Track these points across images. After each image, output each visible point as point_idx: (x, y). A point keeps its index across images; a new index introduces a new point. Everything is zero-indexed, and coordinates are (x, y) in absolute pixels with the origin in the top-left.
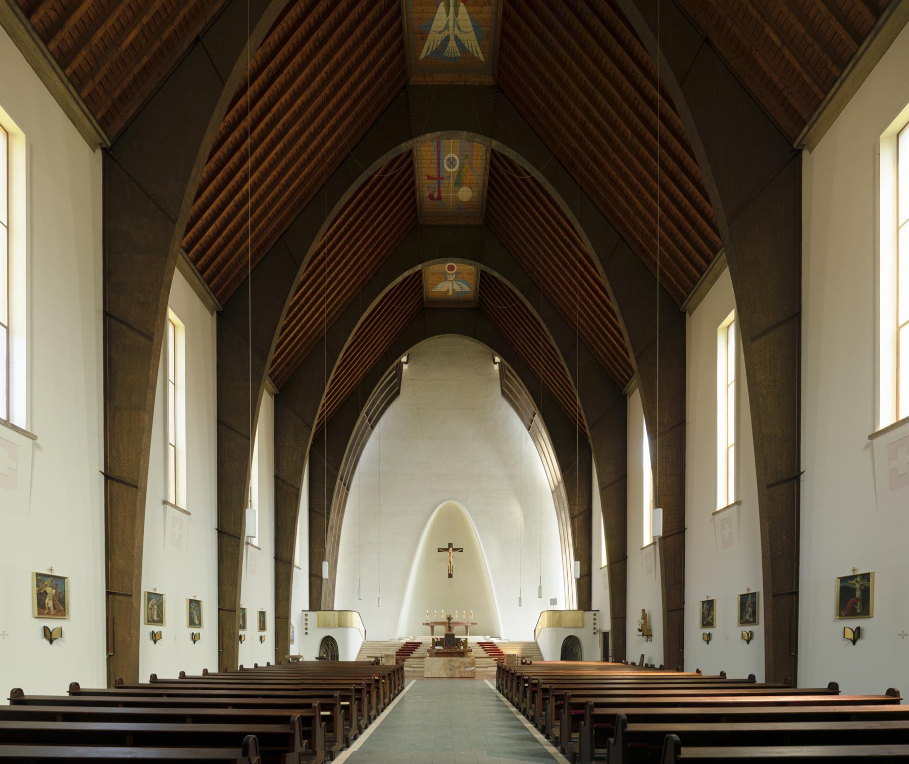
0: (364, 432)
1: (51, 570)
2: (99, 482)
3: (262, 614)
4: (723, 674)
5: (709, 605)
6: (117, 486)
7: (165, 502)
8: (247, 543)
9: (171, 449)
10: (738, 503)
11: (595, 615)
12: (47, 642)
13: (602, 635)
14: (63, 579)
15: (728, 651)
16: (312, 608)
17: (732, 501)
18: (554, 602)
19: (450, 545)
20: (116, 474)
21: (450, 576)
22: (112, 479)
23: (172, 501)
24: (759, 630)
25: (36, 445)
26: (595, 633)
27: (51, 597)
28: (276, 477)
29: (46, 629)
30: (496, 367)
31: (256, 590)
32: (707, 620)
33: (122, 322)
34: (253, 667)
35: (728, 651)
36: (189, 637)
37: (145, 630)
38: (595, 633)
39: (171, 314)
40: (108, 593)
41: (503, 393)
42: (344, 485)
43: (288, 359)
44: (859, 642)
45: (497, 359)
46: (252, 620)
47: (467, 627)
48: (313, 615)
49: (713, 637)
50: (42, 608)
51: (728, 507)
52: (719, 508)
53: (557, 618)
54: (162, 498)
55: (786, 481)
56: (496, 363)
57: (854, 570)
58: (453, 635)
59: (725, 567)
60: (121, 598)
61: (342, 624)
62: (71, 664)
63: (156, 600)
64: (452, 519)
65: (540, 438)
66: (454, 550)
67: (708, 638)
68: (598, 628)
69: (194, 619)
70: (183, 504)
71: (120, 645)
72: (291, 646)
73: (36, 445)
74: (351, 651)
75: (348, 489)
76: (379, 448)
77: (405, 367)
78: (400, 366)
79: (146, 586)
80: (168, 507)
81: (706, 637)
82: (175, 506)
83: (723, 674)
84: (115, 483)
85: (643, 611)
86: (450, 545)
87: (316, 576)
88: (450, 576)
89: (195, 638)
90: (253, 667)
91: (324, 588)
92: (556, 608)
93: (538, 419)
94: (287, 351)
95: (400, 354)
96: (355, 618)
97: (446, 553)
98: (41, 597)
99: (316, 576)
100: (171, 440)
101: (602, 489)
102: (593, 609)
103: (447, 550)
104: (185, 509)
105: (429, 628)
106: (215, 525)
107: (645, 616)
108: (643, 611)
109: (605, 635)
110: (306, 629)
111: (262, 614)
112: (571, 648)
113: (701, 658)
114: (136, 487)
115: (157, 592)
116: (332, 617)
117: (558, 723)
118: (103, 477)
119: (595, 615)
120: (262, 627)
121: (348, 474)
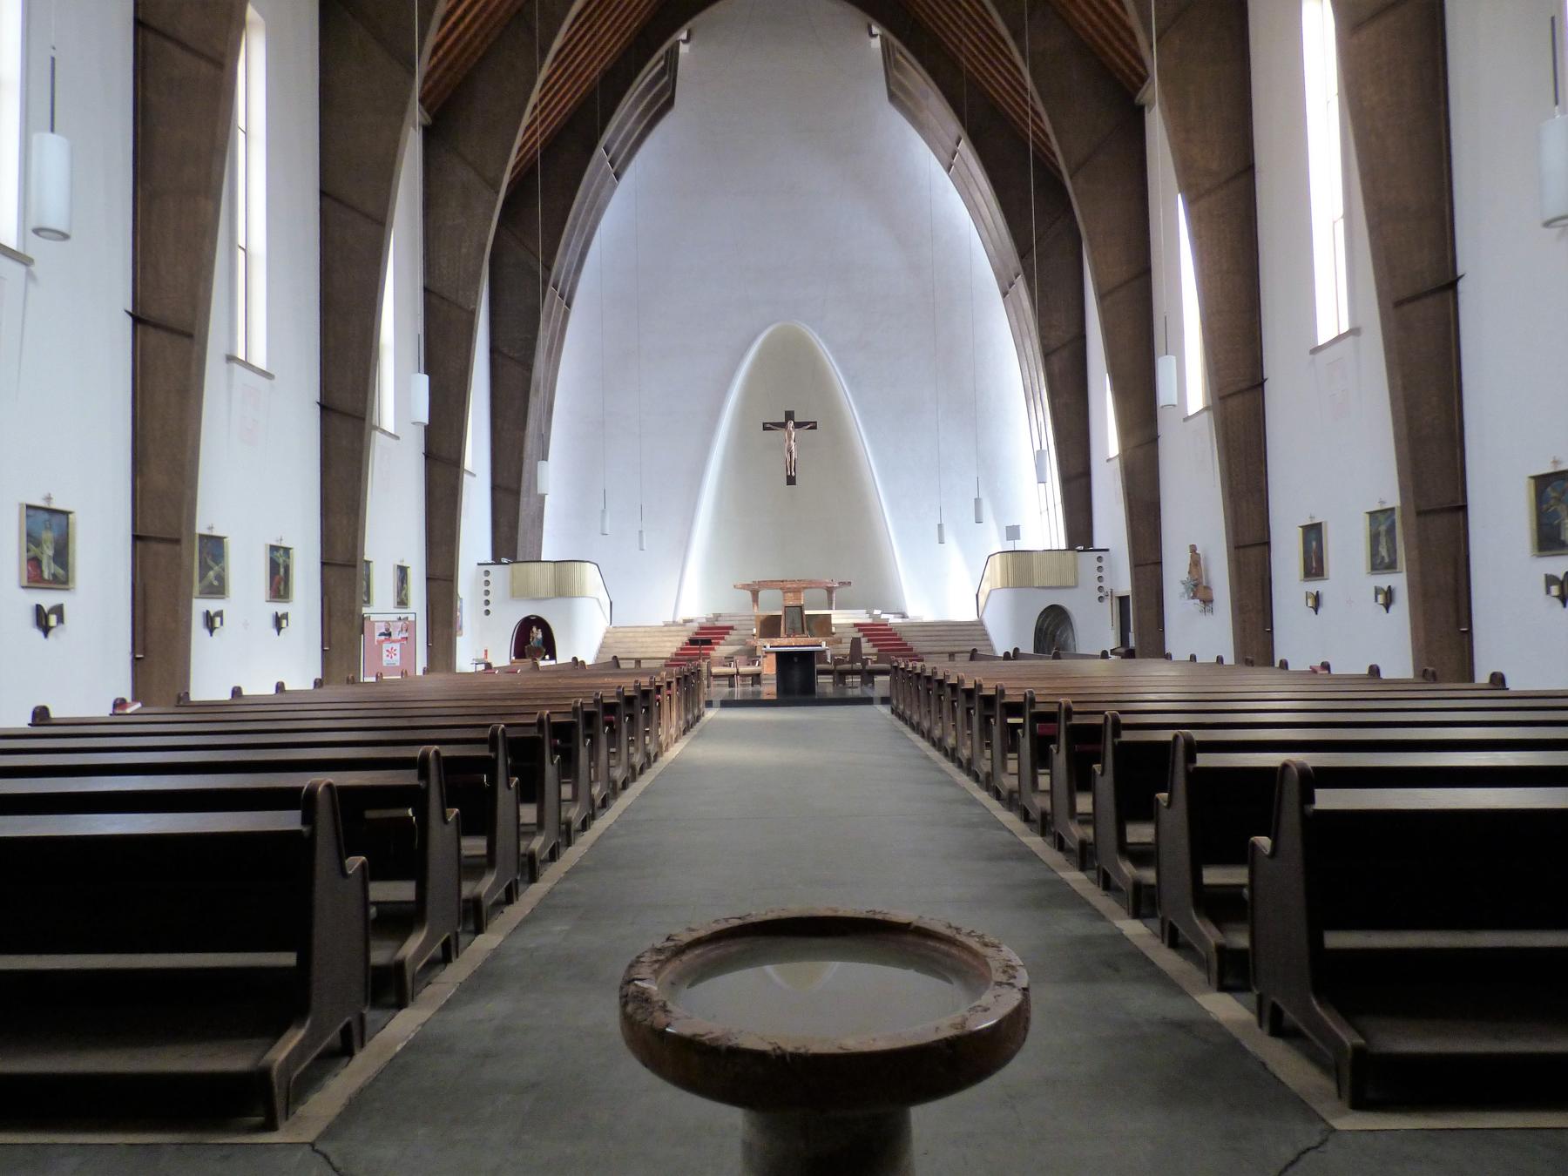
0: (601, 186)
1: (49, 499)
2: (316, 412)
3: (403, 571)
4: (1374, 671)
5: (1313, 533)
6: (154, 337)
7: (231, 358)
8: (376, 428)
9: (241, 254)
10: (1354, 331)
11: (1100, 559)
12: (40, 634)
13: (1116, 603)
14: (66, 513)
15: (1350, 628)
16: (496, 559)
17: (1345, 328)
18: (1013, 532)
19: (789, 415)
20: (154, 312)
21: (791, 481)
22: (334, 411)
23: (241, 355)
24: (1398, 581)
25: (30, 276)
26: (1101, 599)
27: (48, 548)
28: (427, 290)
29: (39, 608)
30: (876, 43)
31: (256, 483)
32: (1314, 567)
33: (352, 208)
34: (227, 696)
35: (1350, 628)
36: (29, 617)
37: (200, 606)
38: (1101, 599)
39: (251, 13)
40: (136, 538)
41: (892, 97)
42: (561, 296)
43: (452, 56)
44: (1392, 608)
45: (875, 30)
46: (246, 571)
47: (830, 590)
48: (500, 573)
49: (1325, 600)
50: (35, 577)
51: (1340, 338)
52: (1323, 337)
53: (1020, 566)
54: (224, 351)
55: (1433, 292)
56: (873, 36)
57: (1382, 502)
58: (801, 608)
59: (1337, 458)
60: (161, 547)
61: (563, 588)
62: (82, 672)
63: (214, 546)
64: (791, 363)
65: (973, 188)
66: (798, 425)
67: (1317, 602)
68: (1107, 589)
69: (279, 584)
70: (259, 359)
71: (158, 640)
72: (459, 639)
73: (30, 276)
74: (582, 639)
75: (569, 305)
76: (629, 216)
77: (684, 49)
78: (673, 54)
79: (201, 528)
80: (236, 366)
81: (1381, 598)
82: (246, 364)
83: (1374, 671)
84: (151, 330)
85: (1193, 549)
86: (789, 415)
87: (345, 414)
88: (791, 481)
89: (279, 622)
90: (227, 696)
91: (522, 514)
92: (1021, 545)
93: (965, 147)
94: (449, 43)
95: (675, 28)
96: (590, 576)
97: (781, 433)
98: (62, 554)
99: (345, 414)
100: (241, 241)
101: (1101, 297)
102: (1098, 544)
103: (783, 425)
104: (264, 368)
105: (748, 594)
106: (316, 395)
107: (1196, 562)
108: (1193, 549)
109: (1123, 600)
110: (487, 602)
111: (403, 571)
112: (1053, 629)
113: (1299, 637)
114: (190, 336)
115: (54, 506)
116: (539, 576)
117: (988, 753)
118: (129, 320)
119: (1100, 559)
120: (279, 584)
121: (568, 272)
